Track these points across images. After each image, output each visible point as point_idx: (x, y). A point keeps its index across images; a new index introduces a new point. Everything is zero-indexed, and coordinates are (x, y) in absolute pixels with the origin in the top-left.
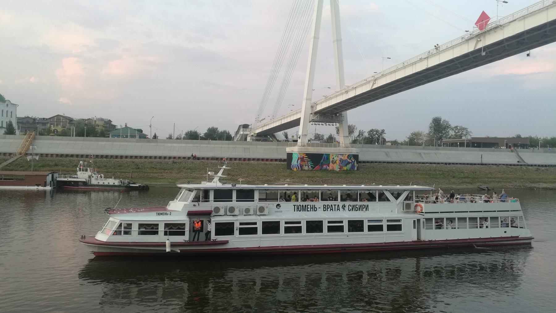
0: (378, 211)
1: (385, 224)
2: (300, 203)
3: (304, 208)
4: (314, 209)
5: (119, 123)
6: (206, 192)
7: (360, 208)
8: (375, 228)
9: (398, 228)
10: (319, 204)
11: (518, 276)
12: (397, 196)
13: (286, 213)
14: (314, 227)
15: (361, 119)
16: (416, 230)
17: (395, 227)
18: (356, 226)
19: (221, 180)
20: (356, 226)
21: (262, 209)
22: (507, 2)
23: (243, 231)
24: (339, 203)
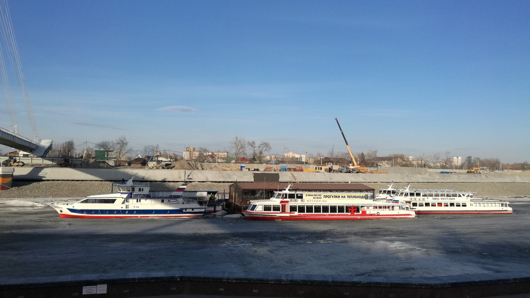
0: (457, 200)
1: (461, 205)
2: (434, 197)
3: (435, 199)
4: (438, 199)
5: (503, 161)
7: (452, 199)
8: (458, 205)
9: (465, 206)
11: (63, 157)
13: (430, 200)
14: (440, 204)
16: (304, 194)
17: (464, 205)
18: (452, 205)
19: (289, 190)
20: (452, 205)
21: (424, 199)
22: (336, 119)
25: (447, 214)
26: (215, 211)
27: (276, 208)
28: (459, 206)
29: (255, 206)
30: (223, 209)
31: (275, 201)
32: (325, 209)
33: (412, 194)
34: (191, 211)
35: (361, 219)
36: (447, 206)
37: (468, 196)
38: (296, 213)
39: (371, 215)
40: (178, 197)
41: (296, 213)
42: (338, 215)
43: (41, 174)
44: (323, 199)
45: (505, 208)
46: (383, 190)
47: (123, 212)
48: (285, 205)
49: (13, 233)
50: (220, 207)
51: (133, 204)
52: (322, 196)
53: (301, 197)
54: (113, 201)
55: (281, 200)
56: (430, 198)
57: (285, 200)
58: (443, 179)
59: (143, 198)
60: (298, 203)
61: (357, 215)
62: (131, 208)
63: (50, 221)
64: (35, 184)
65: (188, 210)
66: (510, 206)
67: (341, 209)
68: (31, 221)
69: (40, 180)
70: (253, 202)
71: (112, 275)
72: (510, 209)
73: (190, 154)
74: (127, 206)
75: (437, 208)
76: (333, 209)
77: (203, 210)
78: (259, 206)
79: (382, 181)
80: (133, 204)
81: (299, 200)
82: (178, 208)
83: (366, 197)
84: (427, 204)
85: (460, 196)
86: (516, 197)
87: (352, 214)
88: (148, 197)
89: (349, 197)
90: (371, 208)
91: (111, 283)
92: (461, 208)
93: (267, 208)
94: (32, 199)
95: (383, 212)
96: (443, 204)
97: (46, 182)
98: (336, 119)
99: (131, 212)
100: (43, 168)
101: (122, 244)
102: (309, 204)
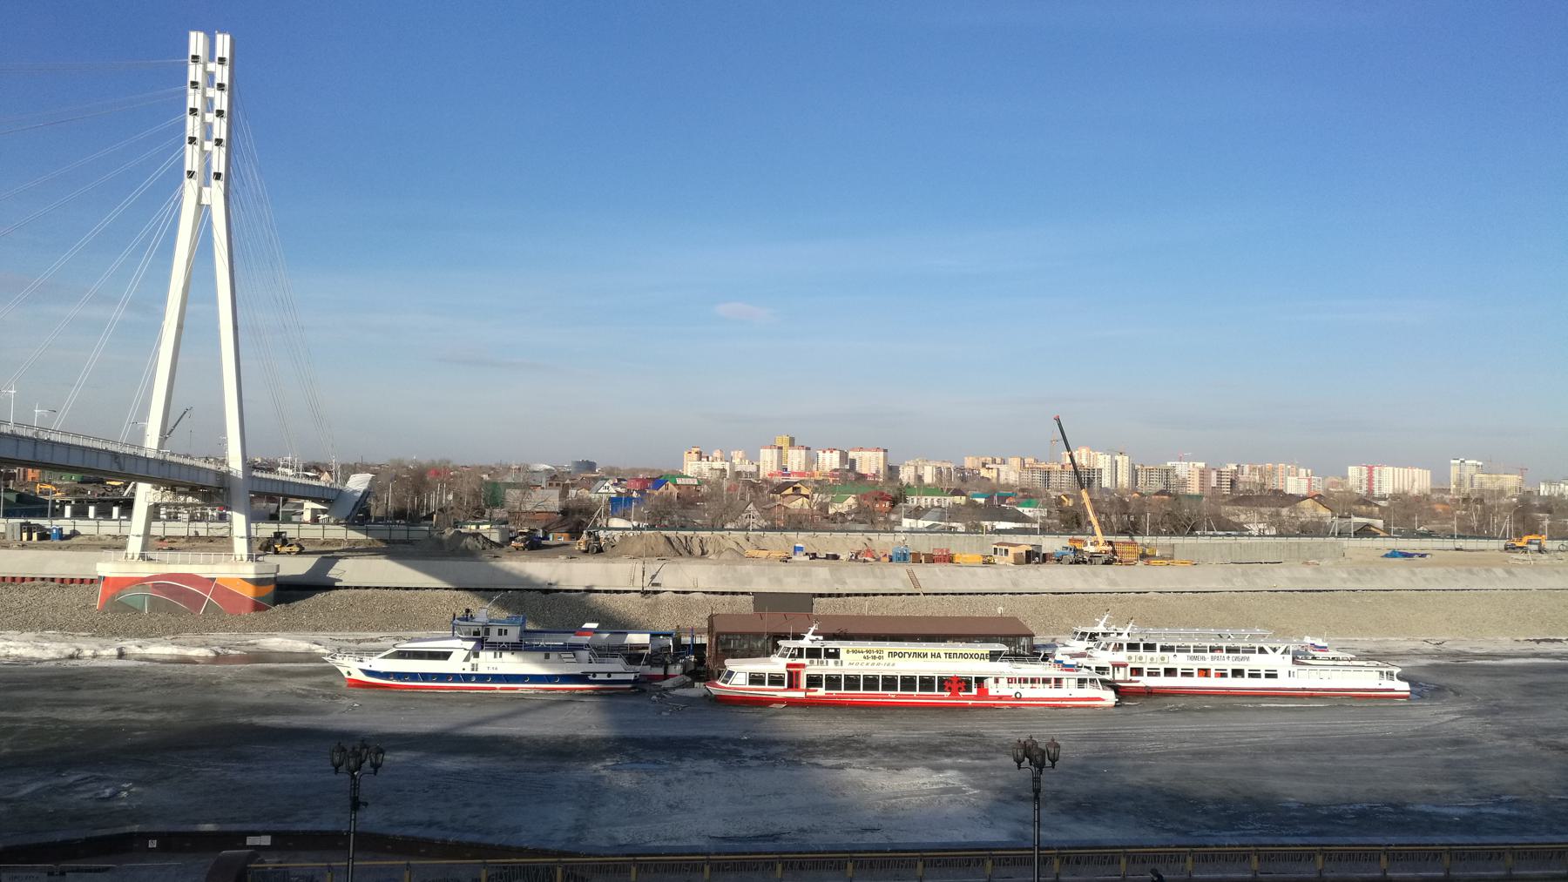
1: (1263, 673)
3: (1196, 658)
4: (1204, 658)
6: (800, 650)
8: (1254, 675)
9: (1275, 676)
10: (1208, 655)
12: (1275, 650)
15: (600, 597)
17: (1271, 675)
20: (1237, 673)
22: (1058, 419)
23: (1149, 674)
24: (1225, 654)
25: (1225, 695)
26: (666, 677)
27: (776, 680)
28: (1258, 676)
29: (731, 674)
30: (684, 673)
31: (776, 665)
32: (890, 682)
33: (1133, 647)
34: (605, 677)
35: (975, 707)
36: (1224, 675)
37: (1286, 652)
38: (821, 692)
39: (1000, 698)
40: (579, 647)
41: (821, 692)
42: (919, 697)
43: (332, 573)
44: (887, 659)
45: (1387, 684)
46: (1081, 630)
47: (467, 678)
48: (798, 673)
49: (252, 725)
50: (679, 667)
51: (489, 662)
52: (885, 654)
53: (835, 655)
54: (445, 656)
55: (790, 661)
56: (1182, 656)
57: (799, 661)
58: (1359, 580)
59: (507, 650)
60: (827, 668)
61: (969, 697)
62: (482, 670)
63: (324, 696)
64: (320, 596)
65: (598, 677)
66: (1401, 678)
67: (927, 683)
68: (292, 693)
69: (330, 586)
70: (731, 665)
71: (280, 827)
72: (1404, 686)
73: (780, 458)
74: (474, 667)
75: (1196, 682)
76: (908, 683)
77: (632, 677)
78: (739, 674)
79: (1162, 587)
80: (489, 662)
81: (831, 661)
82: (578, 672)
83: (994, 656)
84: (1170, 672)
85: (1262, 650)
86: (1538, 642)
87: (954, 695)
88: (515, 648)
89: (949, 655)
90: (1003, 682)
91: (275, 835)
92: (1271, 683)
93: (756, 679)
94: (310, 635)
95: (1027, 691)
96: (1213, 673)
97: (342, 592)
98: (1058, 419)
99: (482, 678)
100: (337, 558)
101: (413, 754)
102: (852, 671)
